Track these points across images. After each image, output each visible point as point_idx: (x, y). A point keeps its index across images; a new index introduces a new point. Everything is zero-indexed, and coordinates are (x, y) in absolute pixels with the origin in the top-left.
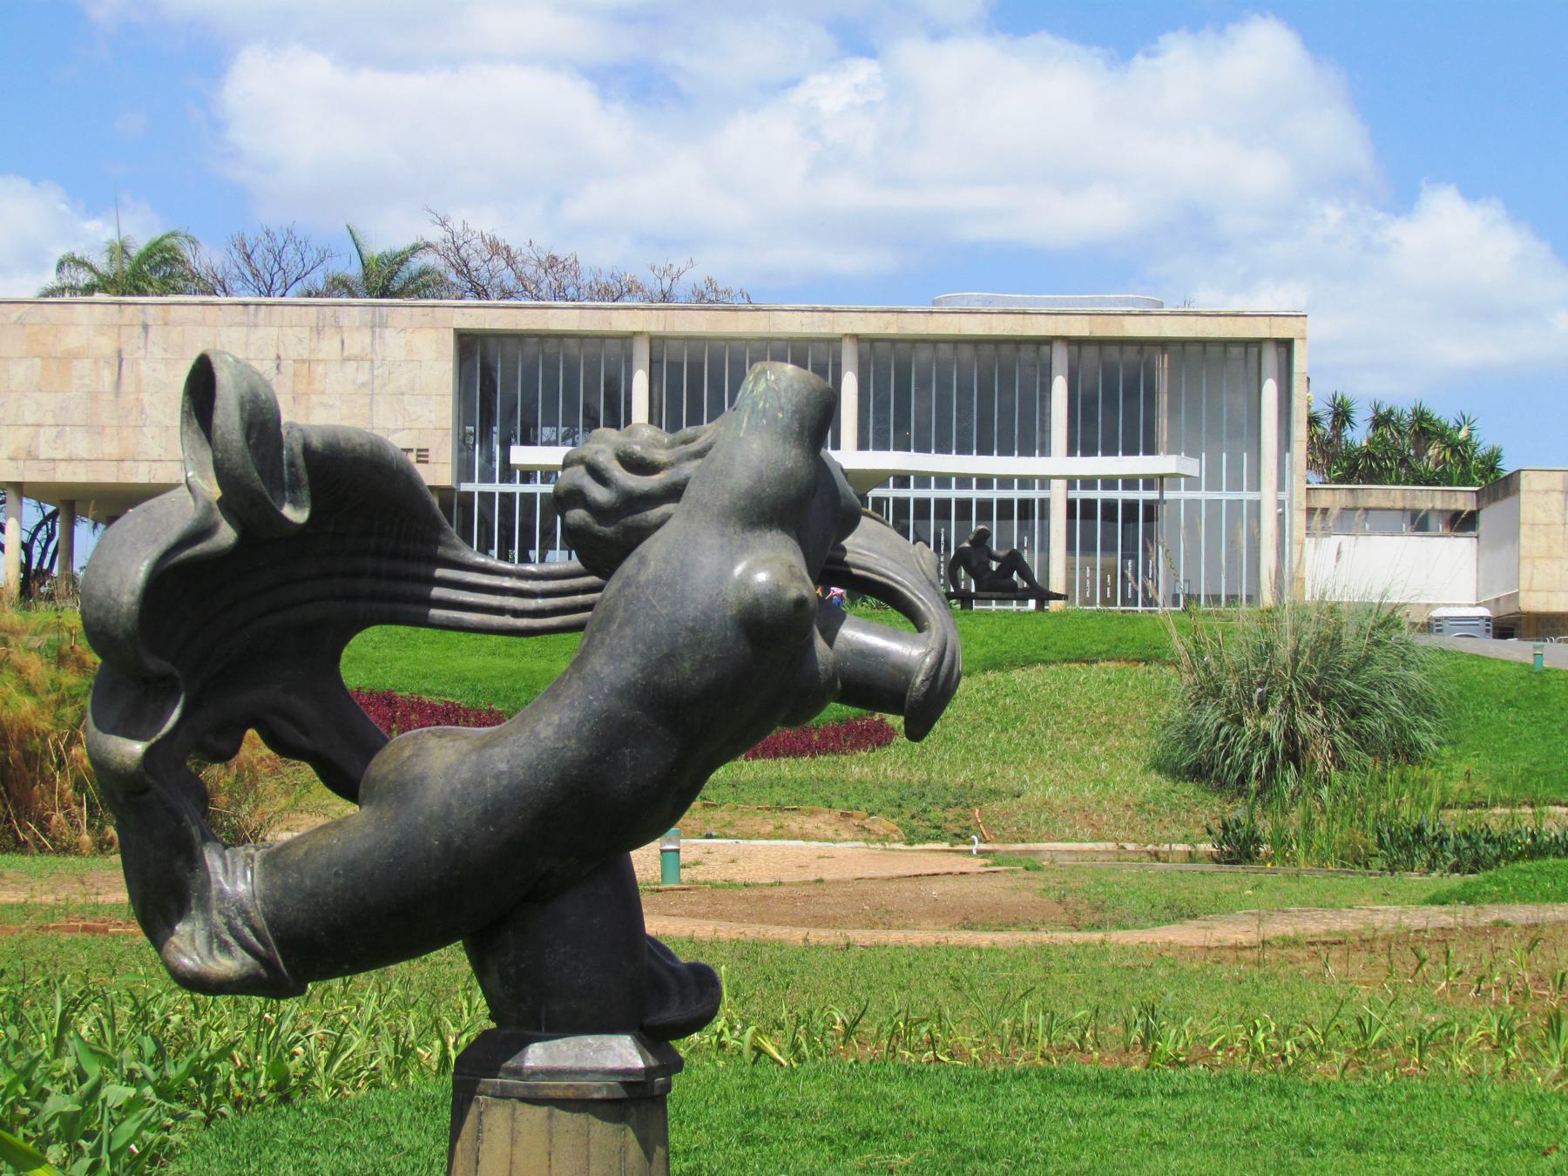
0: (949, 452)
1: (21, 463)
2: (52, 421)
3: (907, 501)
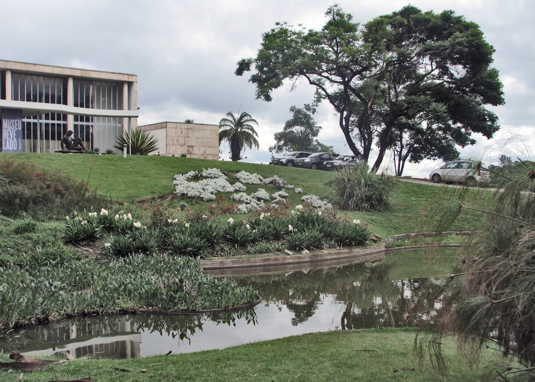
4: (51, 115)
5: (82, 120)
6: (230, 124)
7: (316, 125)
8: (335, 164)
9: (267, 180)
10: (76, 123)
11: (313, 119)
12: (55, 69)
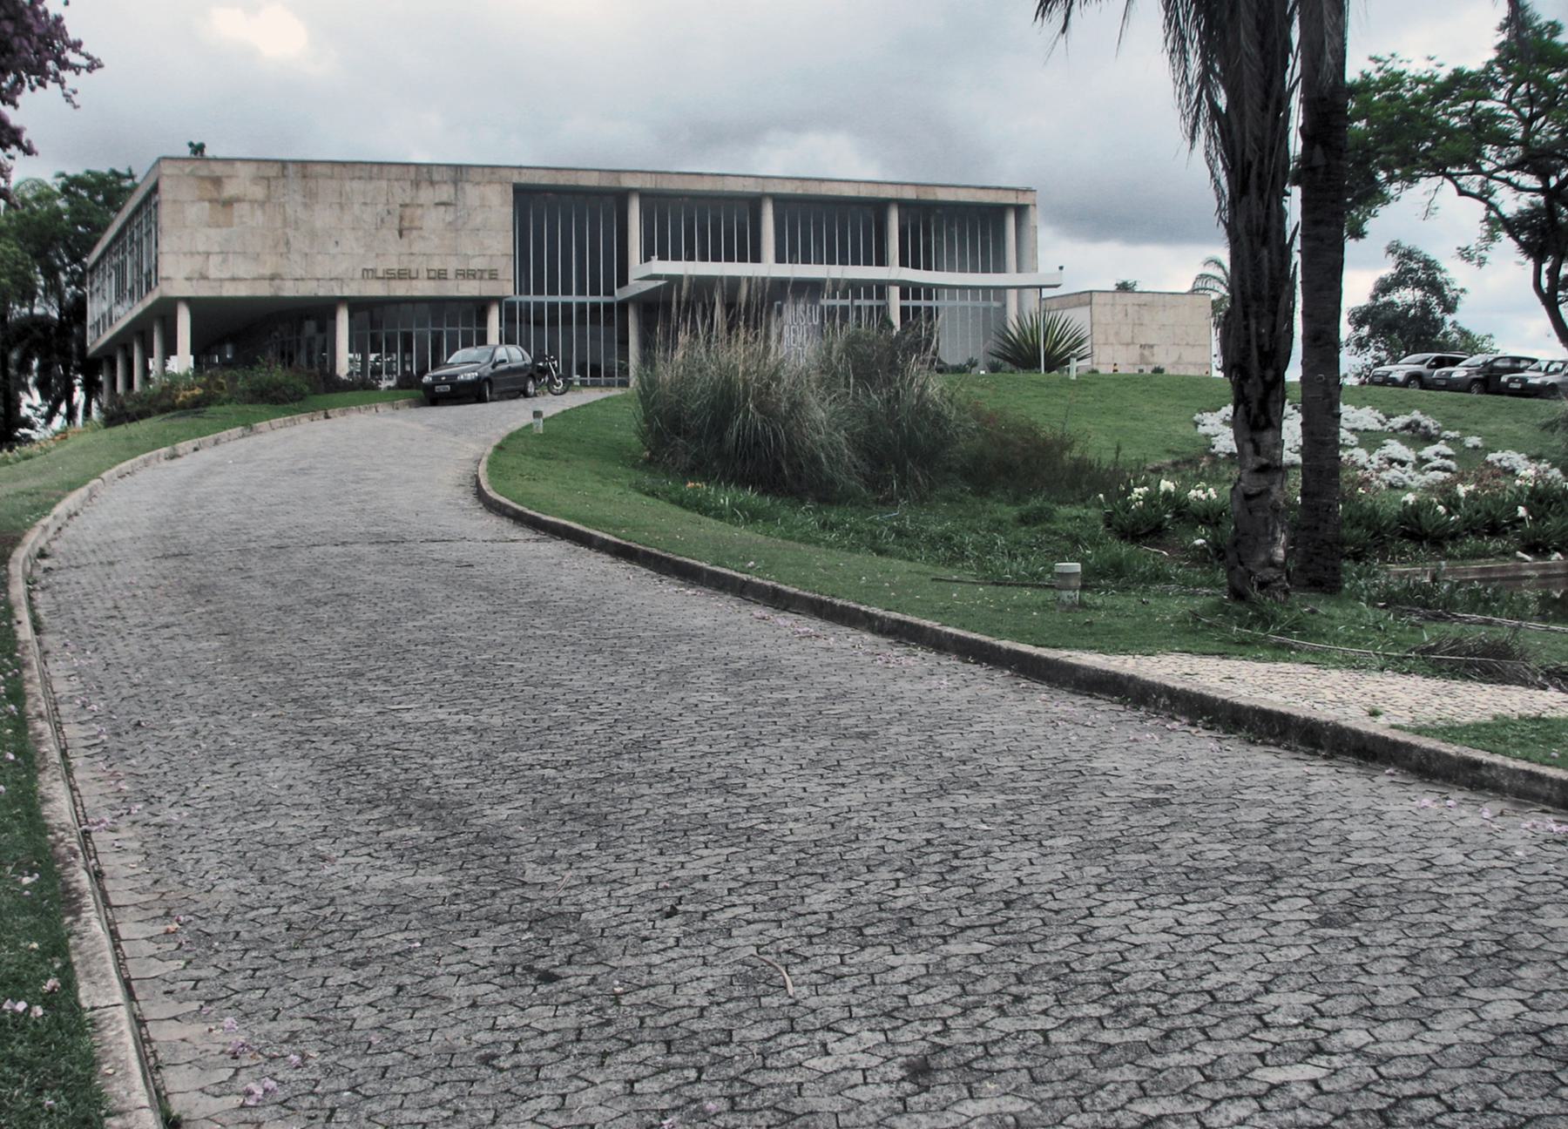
0: (871, 265)
1: (194, 282)
2: (218, 250)
3: (585, 304)
4: (854, 287)
5: (917, 296)
6: (1217, 286)
7: (1452, 287)
8: (1530, 381)
9: (1399, 422)
10: (905, 303)
11: (1445, 271)
12: (862, 186)
